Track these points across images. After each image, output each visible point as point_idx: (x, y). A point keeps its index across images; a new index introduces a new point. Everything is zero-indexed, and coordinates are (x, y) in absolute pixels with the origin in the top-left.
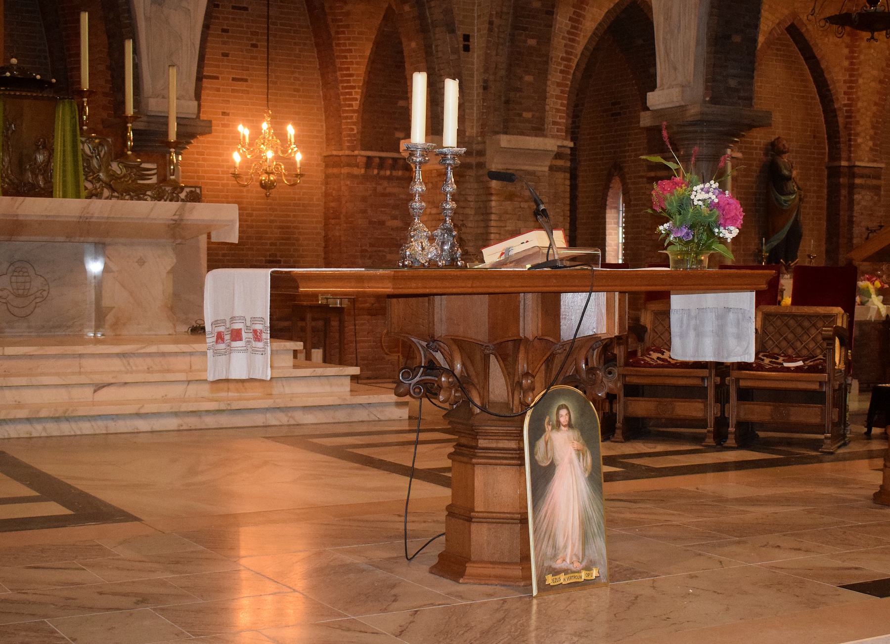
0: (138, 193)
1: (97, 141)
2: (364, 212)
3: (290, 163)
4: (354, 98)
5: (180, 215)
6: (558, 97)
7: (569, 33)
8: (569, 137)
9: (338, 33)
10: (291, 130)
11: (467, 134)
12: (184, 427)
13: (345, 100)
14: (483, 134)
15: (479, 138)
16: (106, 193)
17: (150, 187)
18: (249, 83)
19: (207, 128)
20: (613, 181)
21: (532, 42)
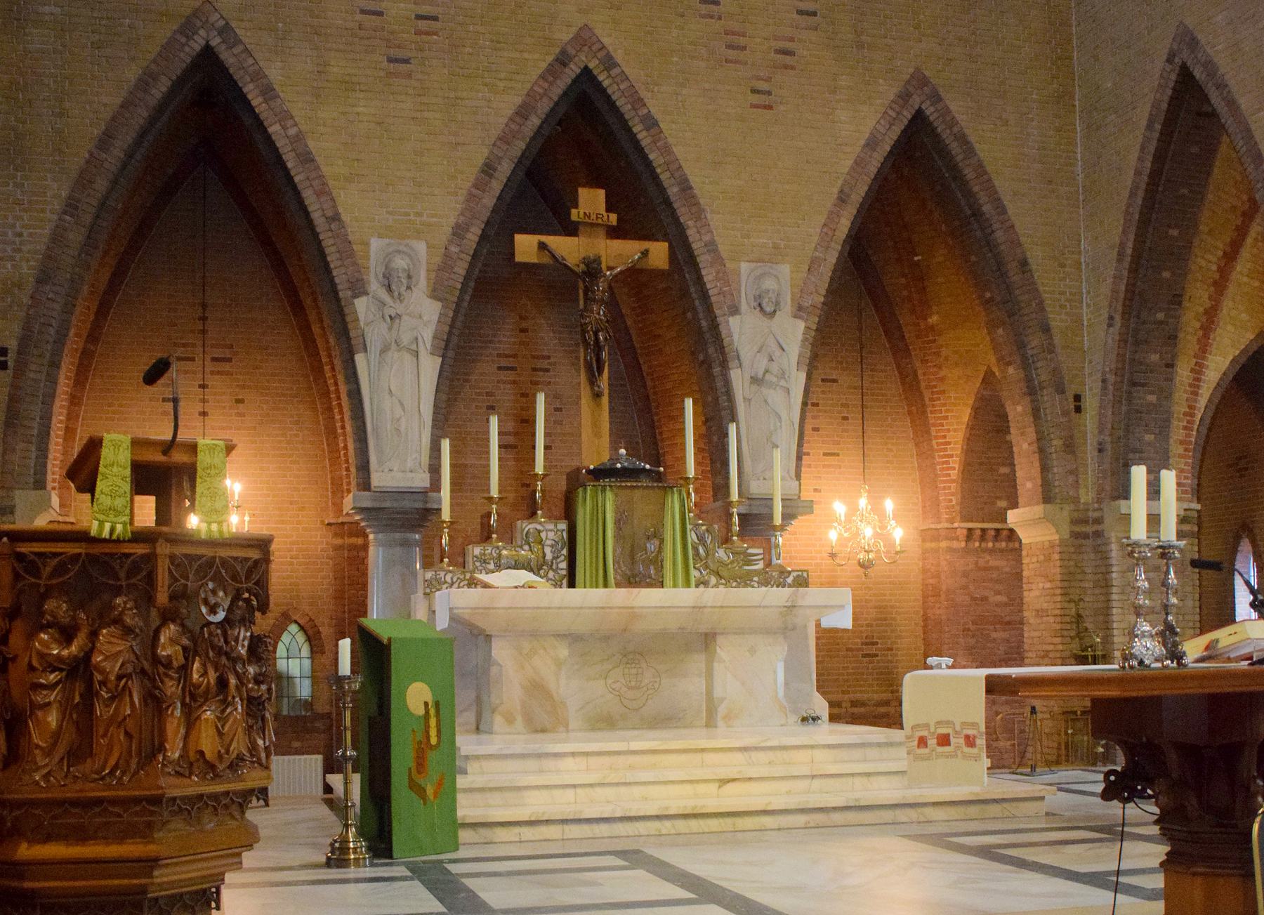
0: (744, 580)
1: (704, 528)
2: (965, 587)
3: (889, 543)
4: (951, 467)
5: (793, 601)
6: (1180, 456)
7: (1190, 385)
8: (1195, 499)
9: (932, 400)
10: (889, 505)
11: (1082, 501)
12: (812, 824)
13: (942, 469)
14: (1099, 501)
15: (1096, 505)
16: (713, 580)
17: (756, 572)
18: (841, 457)
19: (809, 508)
20: (1242, 544)
21: (1152, 398)
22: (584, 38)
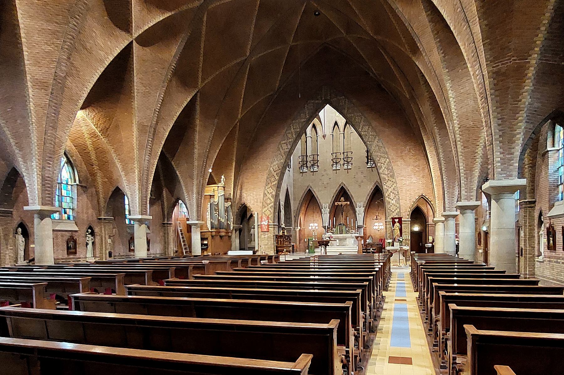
22: (342, 183)
